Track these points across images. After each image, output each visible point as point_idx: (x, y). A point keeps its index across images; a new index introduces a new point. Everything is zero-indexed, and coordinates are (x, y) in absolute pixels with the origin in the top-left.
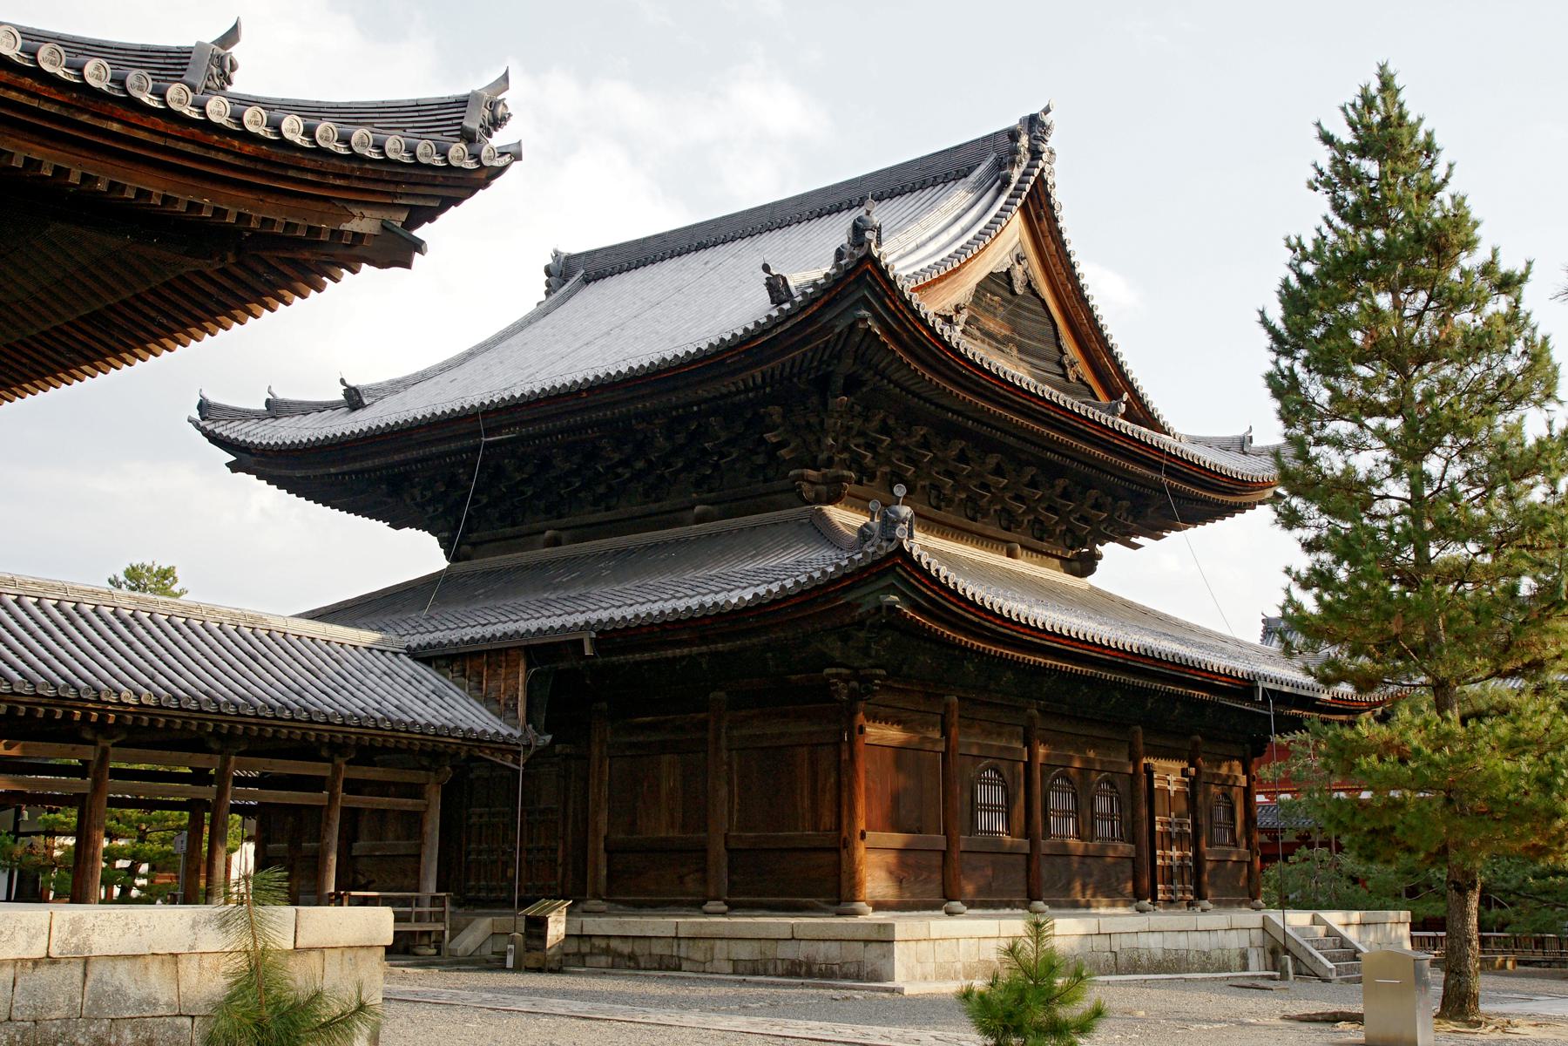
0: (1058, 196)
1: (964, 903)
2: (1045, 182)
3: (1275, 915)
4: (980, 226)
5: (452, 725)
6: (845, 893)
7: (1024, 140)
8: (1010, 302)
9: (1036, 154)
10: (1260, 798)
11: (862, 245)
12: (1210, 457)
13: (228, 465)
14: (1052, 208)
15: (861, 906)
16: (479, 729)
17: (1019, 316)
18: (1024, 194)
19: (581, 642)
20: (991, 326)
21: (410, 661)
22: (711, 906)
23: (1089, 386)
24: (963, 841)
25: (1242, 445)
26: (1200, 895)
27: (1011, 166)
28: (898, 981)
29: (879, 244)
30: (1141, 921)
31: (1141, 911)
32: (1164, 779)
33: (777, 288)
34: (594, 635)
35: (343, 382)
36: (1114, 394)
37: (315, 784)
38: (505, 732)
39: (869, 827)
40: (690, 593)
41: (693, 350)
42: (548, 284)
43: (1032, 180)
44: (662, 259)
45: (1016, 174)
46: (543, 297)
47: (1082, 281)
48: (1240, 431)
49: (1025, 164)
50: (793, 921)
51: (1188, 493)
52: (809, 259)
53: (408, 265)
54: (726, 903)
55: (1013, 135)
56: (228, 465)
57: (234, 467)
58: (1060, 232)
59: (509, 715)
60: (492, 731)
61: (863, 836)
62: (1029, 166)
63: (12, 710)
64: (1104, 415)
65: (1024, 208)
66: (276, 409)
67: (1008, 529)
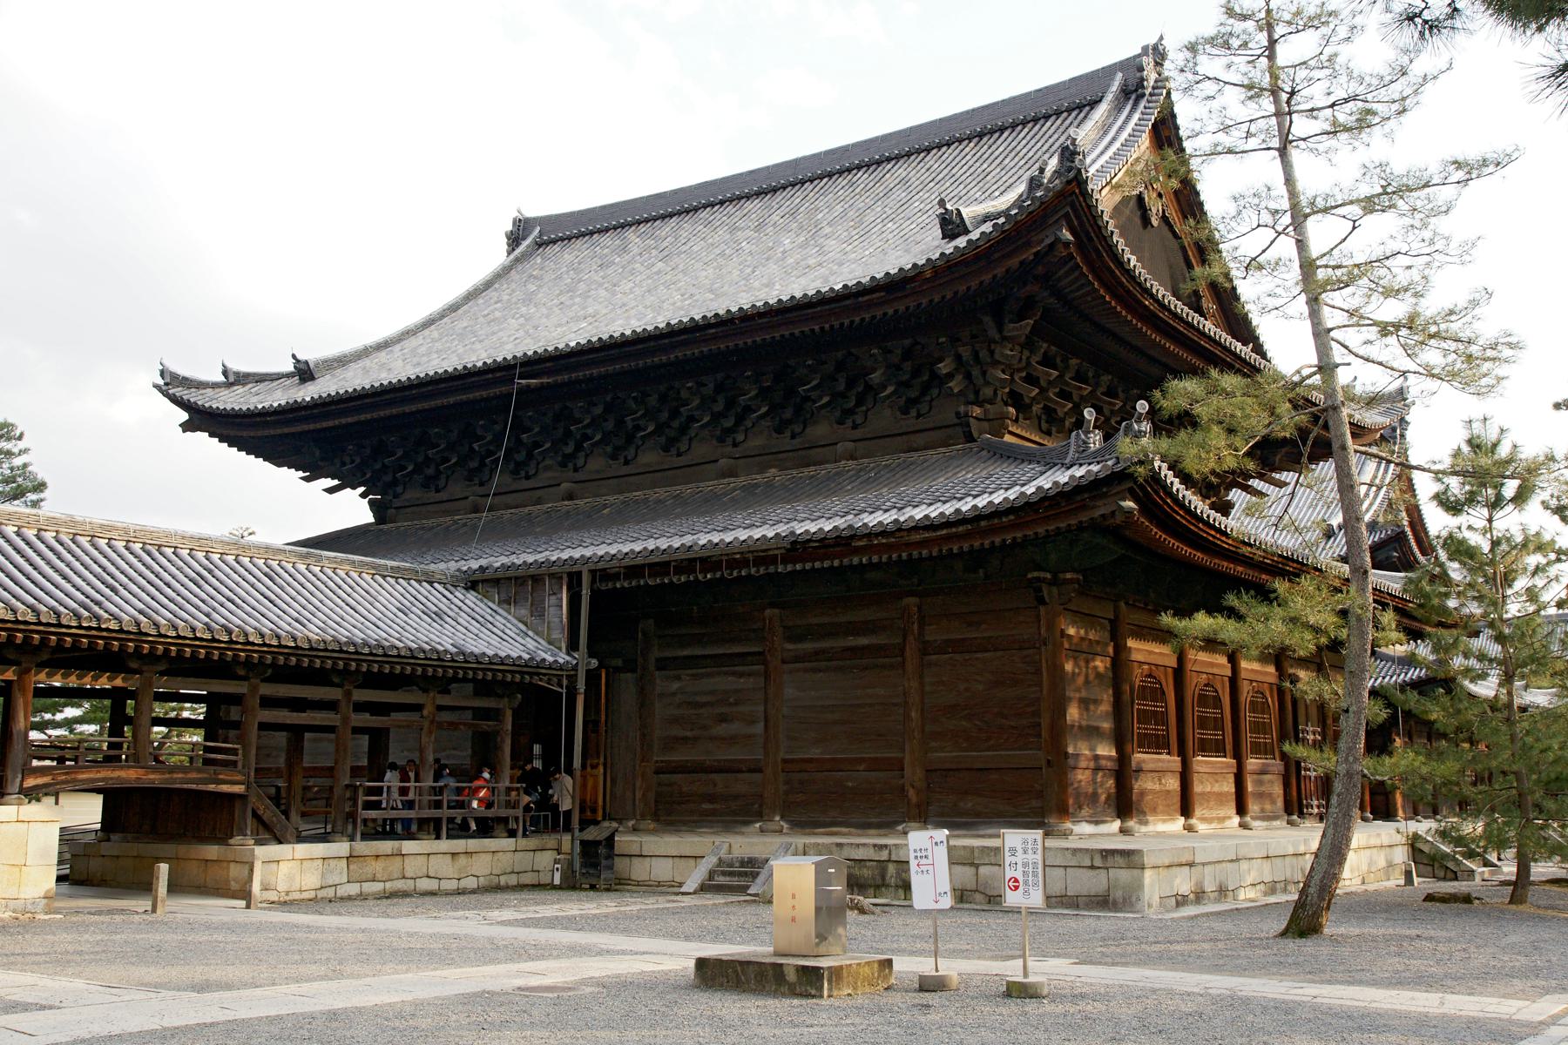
33: (951, 225)
35: (294, 356)
37: (331, 706)
52: (992, 193)
57: (187, 427)
63: (11, 638)
66: (235, 379)
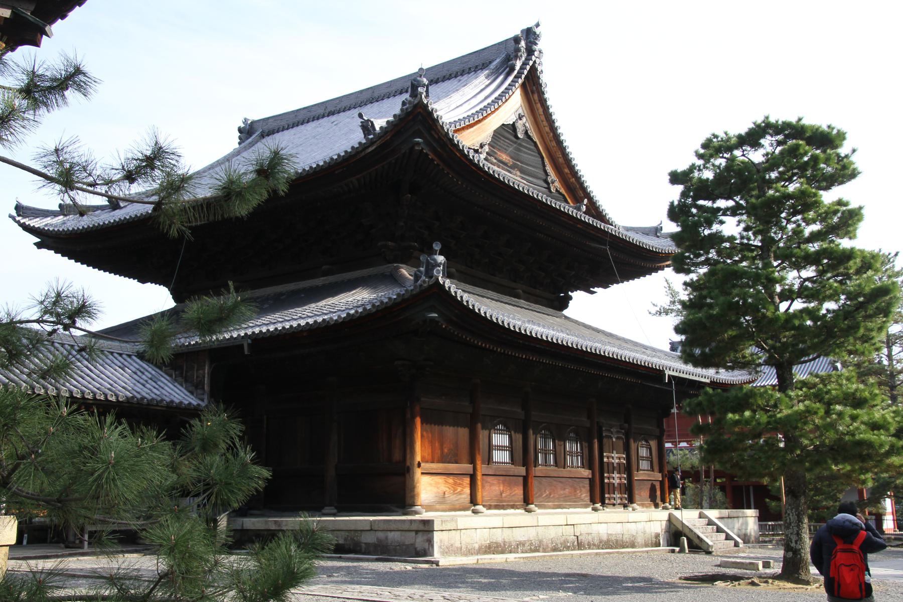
0: (544, 78)
1: (484, 506)
2: (537, 70)
3: (677, 513)
4: (496, 94)
5: (159, 399)
6: (408, 501)
7: (523, 43)
8: (515, 143)
9: (530, 52)
10: (668, 445)
11: (416, 96)
12: (637, 238)
13: (35, 244)
14: (541, 85)
15: (417, 508)
16: (177, 401)
17: (520, 151)
18: (523, 76)
19: (242, 345)
20: (504, 157)
21: (138, 361)
22: (327, 510)
23: (563, 195)
24: (481, 468)
25: (656, 231)
26: (631, 500)
27: (514, 60)
28: (437, 555)
29: (427, 96)
30: (595, 517)
31: (595, 510)
32: (609, 431)
34: (250, 341)
36: (578, 201)
38: (195, 403)
39: (424, 460)
40: (310, 314)
41: (314, 166)
42: (240, 138)
43: (528, 67)
44: (308, 122)
45: (518, 64)
46: (237, 146)
47: (559, 131)
48: (654, 224)
49: (523, 59)
50: (371, 518)
51: (624, 259)
53: (37, 44)
54: (336, 508)
55: (516, 40)
56: (35, 244)
57: (39, 246)
58: (545, 101)
59: (199, 391)
60: (186, 402)
61: (419, 465)
62: (526, 59)
64: (571, 209)
65: (523, 86)
67: (515, 282)
